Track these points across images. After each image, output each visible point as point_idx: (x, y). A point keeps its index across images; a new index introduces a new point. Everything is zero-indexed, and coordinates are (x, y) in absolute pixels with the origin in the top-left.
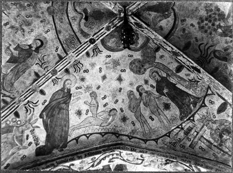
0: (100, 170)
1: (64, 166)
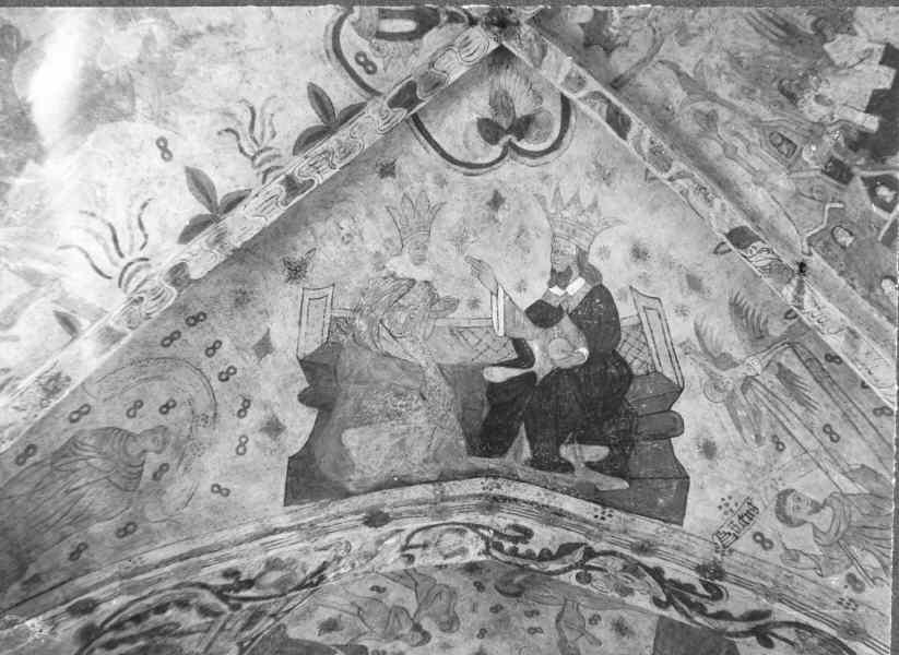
0: (571, 442)
1: (688, 617)
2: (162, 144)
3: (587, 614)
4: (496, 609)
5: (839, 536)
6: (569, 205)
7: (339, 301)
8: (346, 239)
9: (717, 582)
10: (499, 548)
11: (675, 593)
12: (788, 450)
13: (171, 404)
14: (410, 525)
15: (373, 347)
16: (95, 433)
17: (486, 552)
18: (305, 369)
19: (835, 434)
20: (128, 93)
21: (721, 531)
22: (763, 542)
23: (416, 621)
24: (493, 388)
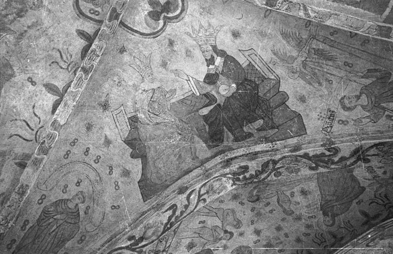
0: (247, 124)
2: (30, 80)
3: (288, 194)
4: (253, 210)
5: (374, 102)
6: (199, 30)
7: (128, 110)
8: (119, 85)
9: (333, 146)
10: (238, 180)
11: (317, 160)
12: (334, 82)
13: (80, 181)
14: (198, 187)
15: (150, 123)
16: (52, 205)
17: (234, 184)
18: (128, 144)
19: (350, 64)
20: (9, 67)
21: (324, 127)
22: (343, 122)
23: (224, 229)
24: (206, 118)
